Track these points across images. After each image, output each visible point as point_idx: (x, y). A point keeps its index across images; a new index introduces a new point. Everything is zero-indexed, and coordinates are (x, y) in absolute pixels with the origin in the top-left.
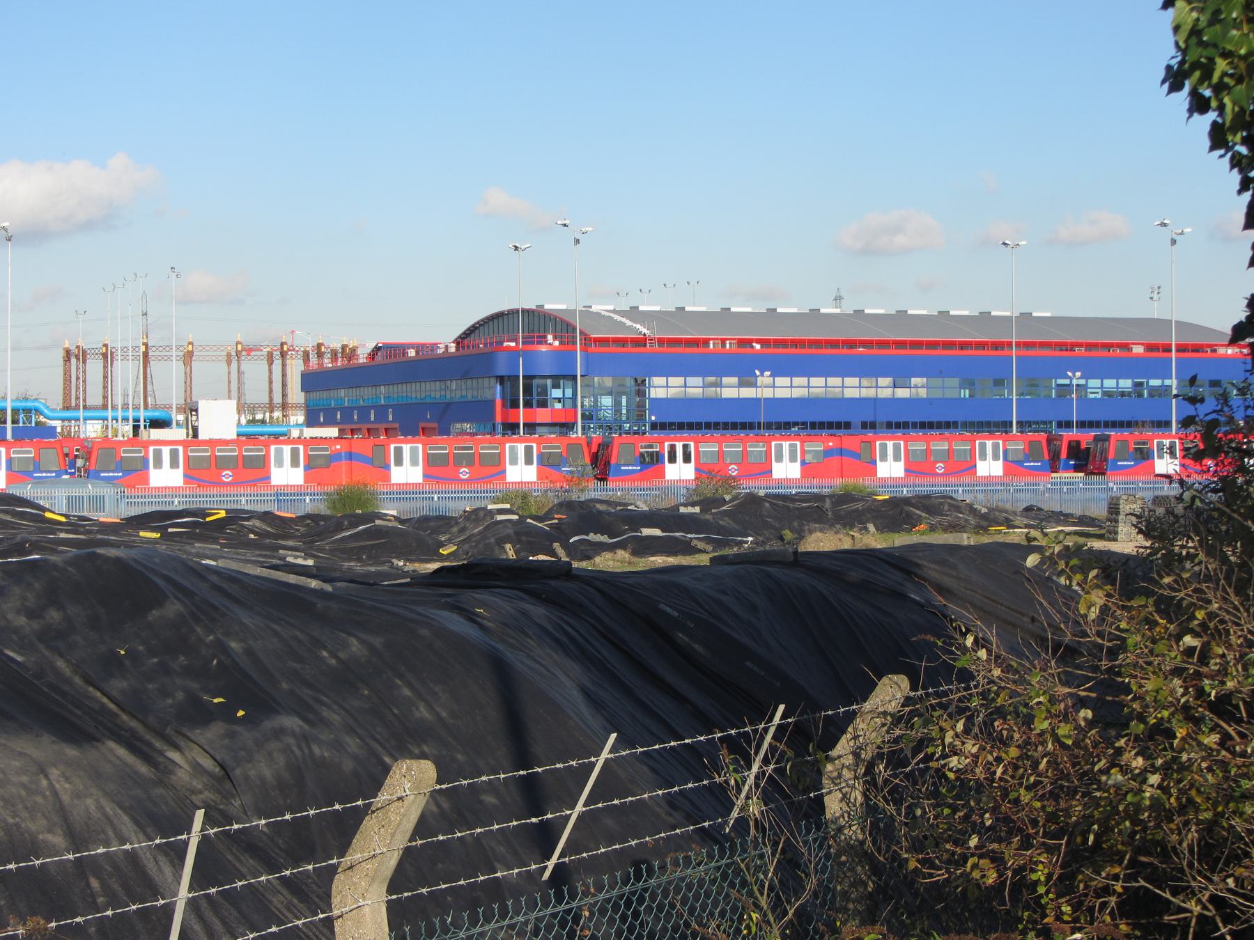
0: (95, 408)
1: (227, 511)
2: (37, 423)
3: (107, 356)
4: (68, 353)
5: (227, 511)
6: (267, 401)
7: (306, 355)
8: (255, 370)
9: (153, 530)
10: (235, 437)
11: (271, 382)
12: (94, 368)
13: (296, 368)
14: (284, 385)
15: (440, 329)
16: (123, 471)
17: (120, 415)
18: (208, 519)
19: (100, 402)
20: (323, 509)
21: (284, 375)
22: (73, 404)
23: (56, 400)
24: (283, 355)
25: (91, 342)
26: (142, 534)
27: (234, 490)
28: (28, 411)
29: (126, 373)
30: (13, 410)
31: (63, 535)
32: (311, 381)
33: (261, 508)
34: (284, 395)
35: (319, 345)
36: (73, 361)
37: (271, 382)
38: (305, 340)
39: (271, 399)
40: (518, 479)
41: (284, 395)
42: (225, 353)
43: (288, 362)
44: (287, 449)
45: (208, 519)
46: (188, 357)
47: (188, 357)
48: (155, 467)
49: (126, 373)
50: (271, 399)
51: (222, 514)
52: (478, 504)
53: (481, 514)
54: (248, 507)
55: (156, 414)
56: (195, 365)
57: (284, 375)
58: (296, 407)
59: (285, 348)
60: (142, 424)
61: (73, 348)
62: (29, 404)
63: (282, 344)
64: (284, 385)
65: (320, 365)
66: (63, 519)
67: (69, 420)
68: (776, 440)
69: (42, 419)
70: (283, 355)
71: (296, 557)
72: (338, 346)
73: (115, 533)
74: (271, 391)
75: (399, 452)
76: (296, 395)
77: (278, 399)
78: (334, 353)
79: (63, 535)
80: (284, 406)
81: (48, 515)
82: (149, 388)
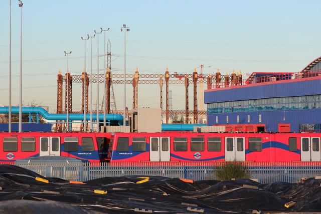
0: (76, 113)
1: (151, 178)
2: (40, 121)
3: (86, 80)
4: (60, 78)
5: (151, 178)
6: (184, 109)
7: (209, 80)
8: (177, 89)
9: (103, 189)
10: (161, 132)
11: (187, 97)
12: (77, 87)
13: (202, 87)
14: (195, 99)
15: (295, 66)
16: (133, 151)
17: (91, 117)
18: (138, 183)
19: (80, 109)
20: (213, 177)
21: (195, 93)
22: (64, 110)
23: (53, 109)
24: (195, 80)
25: (76, 72)
26: (96, 191)
27: (201, 164)
28: (34, 114)
29: (97, 91)
30: (11, 113)
31: (45, 192)
32: (210, 98)
33: (172, 176)
34: (195, 106)
35: (218, 74)
36: (64, 83)
37: (187, 97)
38: (209, 71)
39: (187, 108)
40: (232, 160)
41: (195, 106)
42: (132, 79)
43: (198, 85)
44: (50, 140)
45: (138, 183)
46: (135, 83)
47: (135, 83)
48: (228, 150)
49: (97, 91)
50: (187, 108)
51: (147, 180)
52: (311, 176)
53: (312, 182)
54: (167, 176)
55: (115, 117)
56: (139, 86)
57: (195, 93)
58: (202, 113)
59: (196, 76)
60: (105, 123)
61: (63, 75)
62: (35, 110)
63: (167, 72)
64: (195, 99)
65: (218, 87)
66: (47, 182)
67: (61, 120)
68: (303, 135)
69: (43, 119)
70: (195, 80)
71: (193, 208)
72: (230, 74)
73: (78, 191)
74: (187, 103)
75: (306, 142)
76: (203, 107)
77: (191, 108)
78: (227, 79)
79: (45, 192)
80: (195, 112)
81: (38, 179)
82: (111, 100)
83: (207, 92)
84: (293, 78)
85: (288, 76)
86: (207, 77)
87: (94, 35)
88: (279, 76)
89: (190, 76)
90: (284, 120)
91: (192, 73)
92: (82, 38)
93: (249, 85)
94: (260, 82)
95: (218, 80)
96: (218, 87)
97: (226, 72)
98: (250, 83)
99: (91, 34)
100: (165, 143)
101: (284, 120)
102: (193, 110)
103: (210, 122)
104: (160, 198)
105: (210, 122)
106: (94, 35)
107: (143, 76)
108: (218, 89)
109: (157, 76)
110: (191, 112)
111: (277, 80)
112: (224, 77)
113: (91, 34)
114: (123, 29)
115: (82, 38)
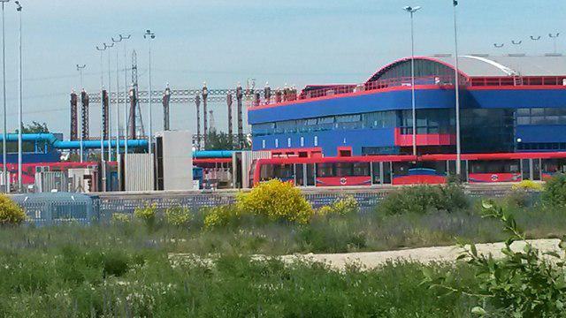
13: (247, 103)
14: (206, 121)
24: (105, 100)
78: (279, 94)
85: (349, 88)
88: (339, 89)
99: (109, 43)
113: (109, 43)
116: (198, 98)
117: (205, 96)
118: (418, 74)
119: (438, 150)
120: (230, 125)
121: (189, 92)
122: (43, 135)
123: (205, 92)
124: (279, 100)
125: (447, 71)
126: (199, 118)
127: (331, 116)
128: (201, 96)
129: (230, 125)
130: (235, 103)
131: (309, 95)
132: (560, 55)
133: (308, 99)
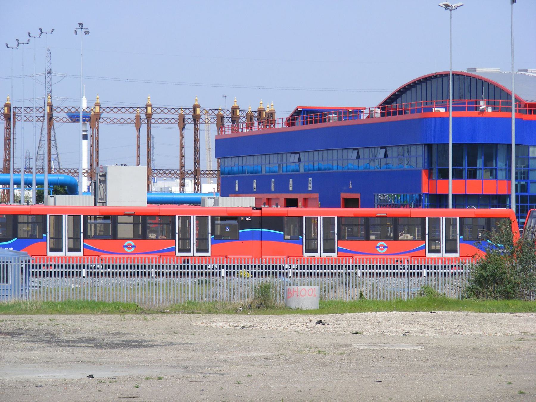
7: (220, 120)
11: (182, 147)
13: (209, 134)
14: (196, 151)
15: (366, 95)
21: (196, 141)
24: (196, 119)
32: (225, 148)
34: (196, 162)
35: (260, 112)
37: (182, 147)
41: (196, 162)
50: (182, 166)
57: (196, 141)
58: (209, 173)
64: (196, 151)
72: (253, 107)
77: (189, 165)
78: (250, 118)
82: (53, 151)
83: (219, 140)
84: (334, 119)
85: (357, 112)
86: (216, 112)
87: (28, 41)
88: (342, 113)
89: (187, 111)
90: (351, 187)
91: (191, 106)
92: (7, 45)
93: (292, 129)
94: (311, 122)
95: (235, 119)
96: (235, 130)
97: (249, 105)
98: (293, 124)
99: (24, 39)
100: (495, 202)
101: (351, 187)
102: (192, 168)
103: (225, 190)
104: (123, 306)
105: (225, 190)
106: (28, 41)
107: (108, 110)
108: (235, 135)
109: (173, 111)
110: (190, 172)
111: (340, 119)
112: (245, 114)
113: (24, 39)
114: (79, 31)
115: (7, 45)
116: (138, 118)
117: (149, 117)
118: (458, 95)
119: (378, 221)
120: (182, 157)
121: (128, 109)
122: (330, 171)
123: (149, 110)
124: (250, 125)
125: (497, 94)
126: (138, 156)
127: (296, 153)
128: (143, 116)
129: (182, 157)
130: (190, 127)
131: (300, 120)
132: (49, 50)
133: (299, 127)
